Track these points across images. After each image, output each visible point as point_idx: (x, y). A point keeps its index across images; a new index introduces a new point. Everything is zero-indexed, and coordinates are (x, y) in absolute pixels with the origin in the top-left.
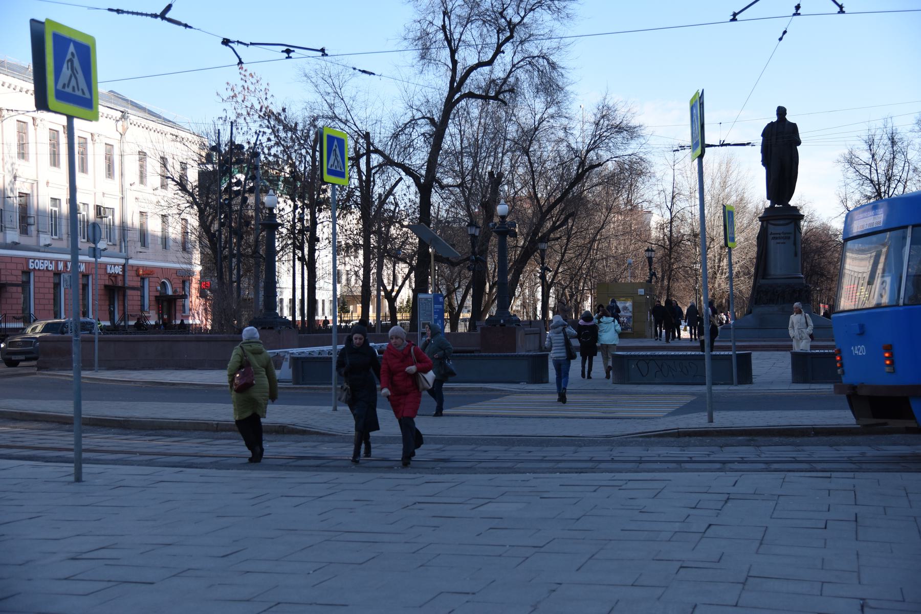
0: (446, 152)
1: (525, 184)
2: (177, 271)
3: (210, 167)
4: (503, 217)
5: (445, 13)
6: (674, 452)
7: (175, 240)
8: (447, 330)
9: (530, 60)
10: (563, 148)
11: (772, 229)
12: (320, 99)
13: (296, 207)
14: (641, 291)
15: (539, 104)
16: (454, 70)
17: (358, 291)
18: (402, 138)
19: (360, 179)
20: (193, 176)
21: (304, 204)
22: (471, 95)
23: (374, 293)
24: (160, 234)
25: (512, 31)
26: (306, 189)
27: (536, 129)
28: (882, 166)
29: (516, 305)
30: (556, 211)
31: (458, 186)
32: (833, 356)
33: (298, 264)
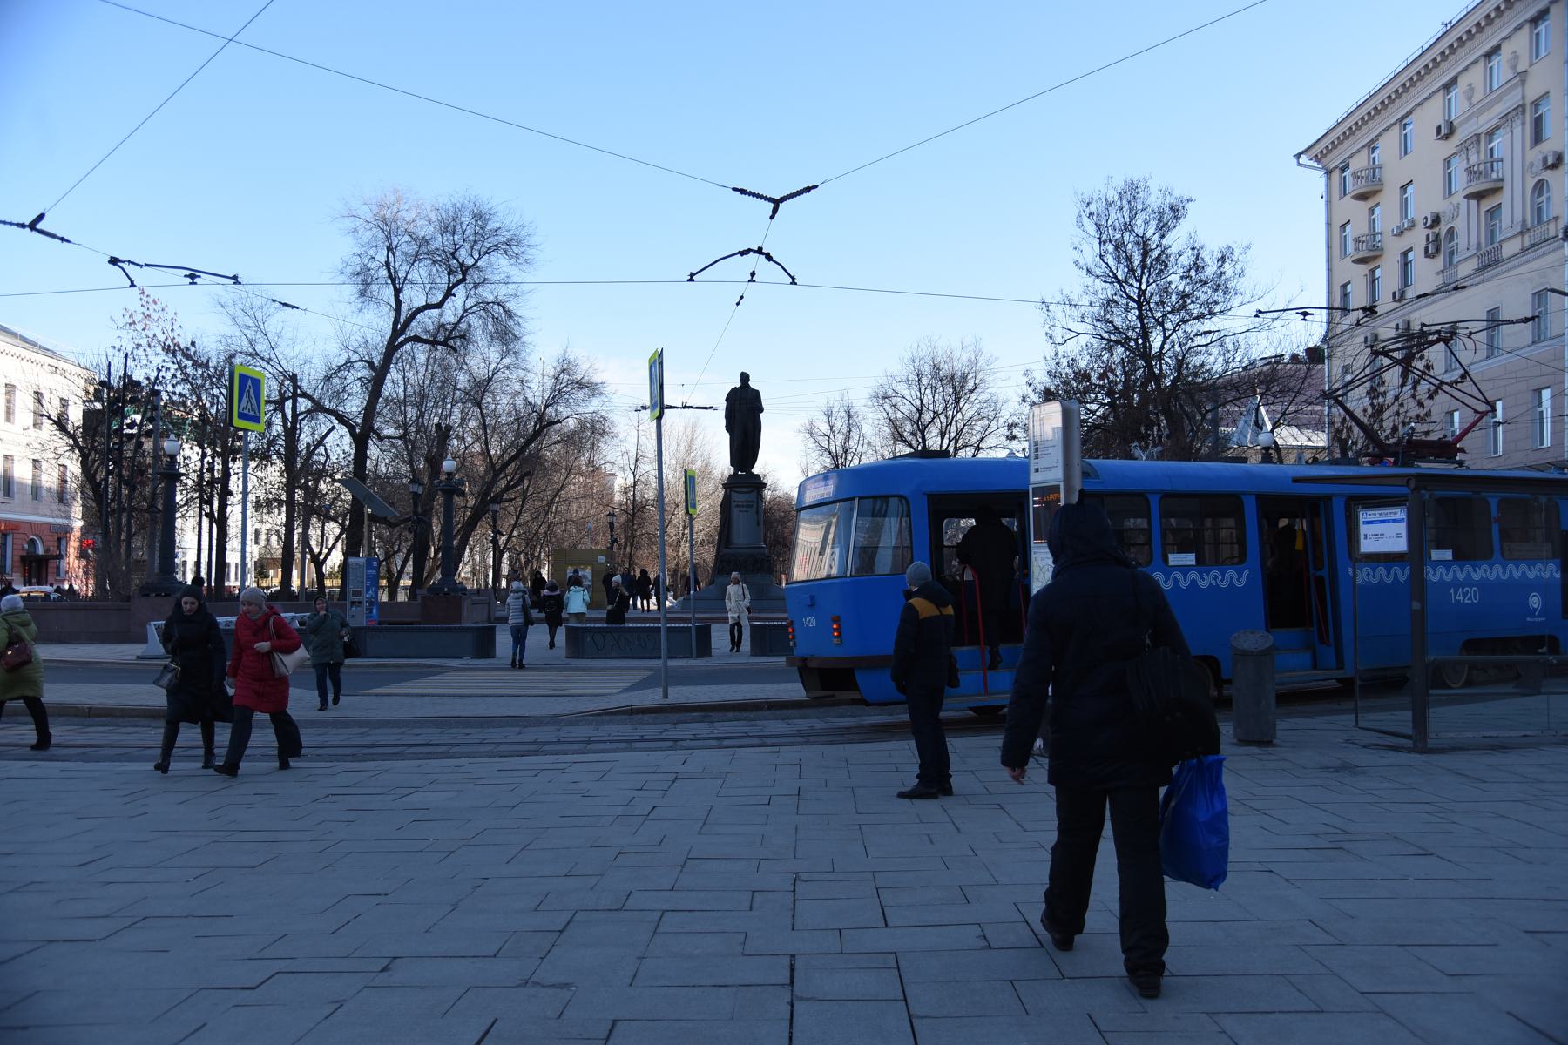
0: (386, 399)
1: (478, 439)
2: (50, 526)
3: (98, 406)
4: (449, 474)
5: (389, 249)
6: (627, 731)
7: (49, 490)
8: (385, 598)
9: (484, 305)
10: (519, 401)
11: (735, 497)
12: (238, 334)
13: (204, 455)
14: (601, 559)
15: (493, 354)
16: (398, 311)
17: (278, 554)
18: (336, 381)
19: (285, 425)
20: (75, 416)
21: (214, 451)
22: (416, 339)
23: (298, 556)
24: (29, 482)
25: (464, 274)
26: (218, 435)
27: (490, 380)
28: (840, 438)
29: (464, 572)
30: (510, 469)
31: (400, 438)
32: (786, 627)
33: (205, 521)
